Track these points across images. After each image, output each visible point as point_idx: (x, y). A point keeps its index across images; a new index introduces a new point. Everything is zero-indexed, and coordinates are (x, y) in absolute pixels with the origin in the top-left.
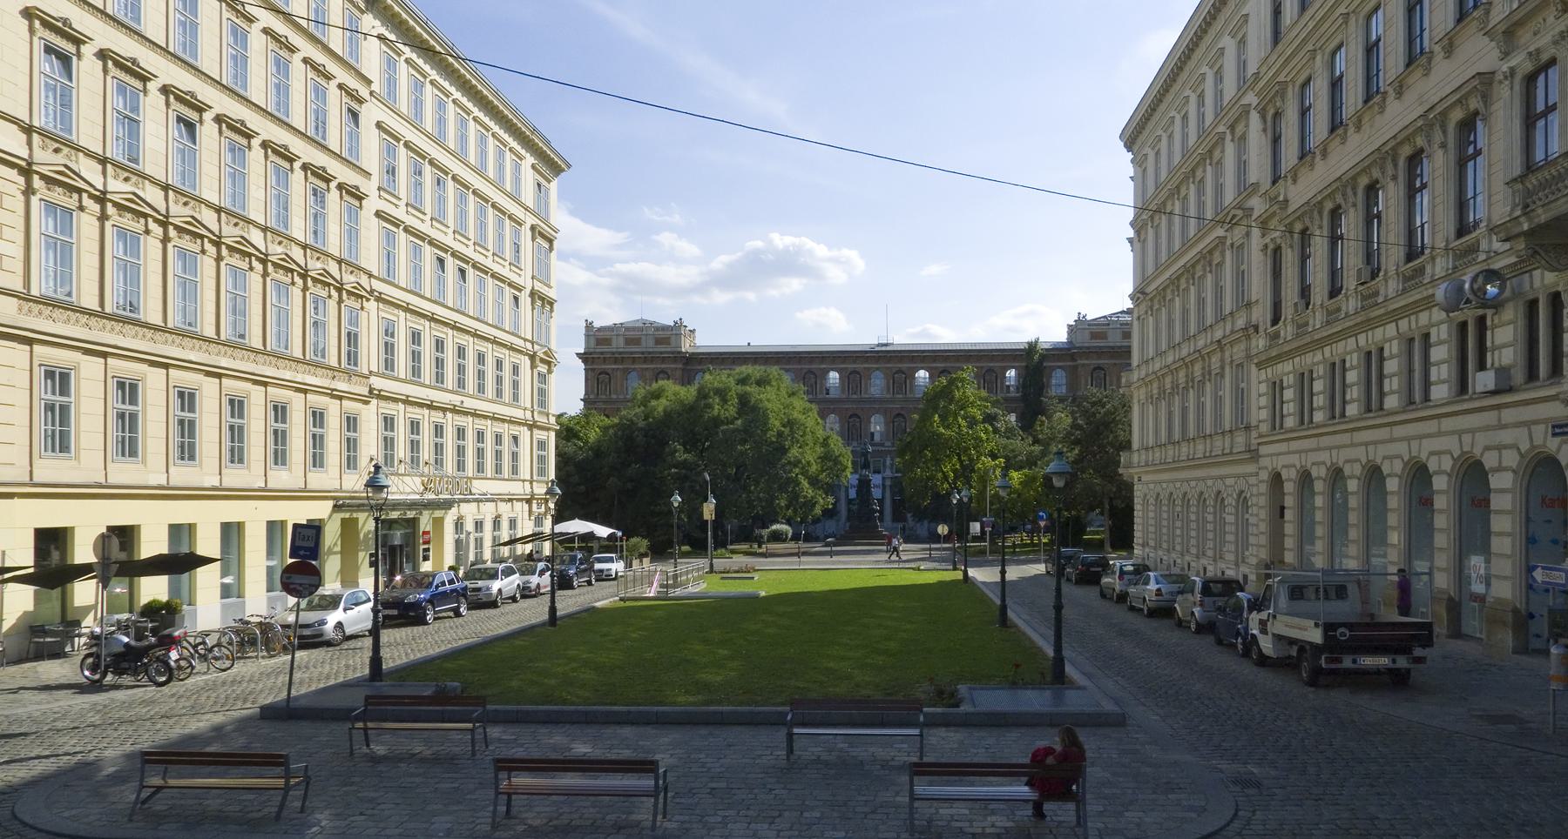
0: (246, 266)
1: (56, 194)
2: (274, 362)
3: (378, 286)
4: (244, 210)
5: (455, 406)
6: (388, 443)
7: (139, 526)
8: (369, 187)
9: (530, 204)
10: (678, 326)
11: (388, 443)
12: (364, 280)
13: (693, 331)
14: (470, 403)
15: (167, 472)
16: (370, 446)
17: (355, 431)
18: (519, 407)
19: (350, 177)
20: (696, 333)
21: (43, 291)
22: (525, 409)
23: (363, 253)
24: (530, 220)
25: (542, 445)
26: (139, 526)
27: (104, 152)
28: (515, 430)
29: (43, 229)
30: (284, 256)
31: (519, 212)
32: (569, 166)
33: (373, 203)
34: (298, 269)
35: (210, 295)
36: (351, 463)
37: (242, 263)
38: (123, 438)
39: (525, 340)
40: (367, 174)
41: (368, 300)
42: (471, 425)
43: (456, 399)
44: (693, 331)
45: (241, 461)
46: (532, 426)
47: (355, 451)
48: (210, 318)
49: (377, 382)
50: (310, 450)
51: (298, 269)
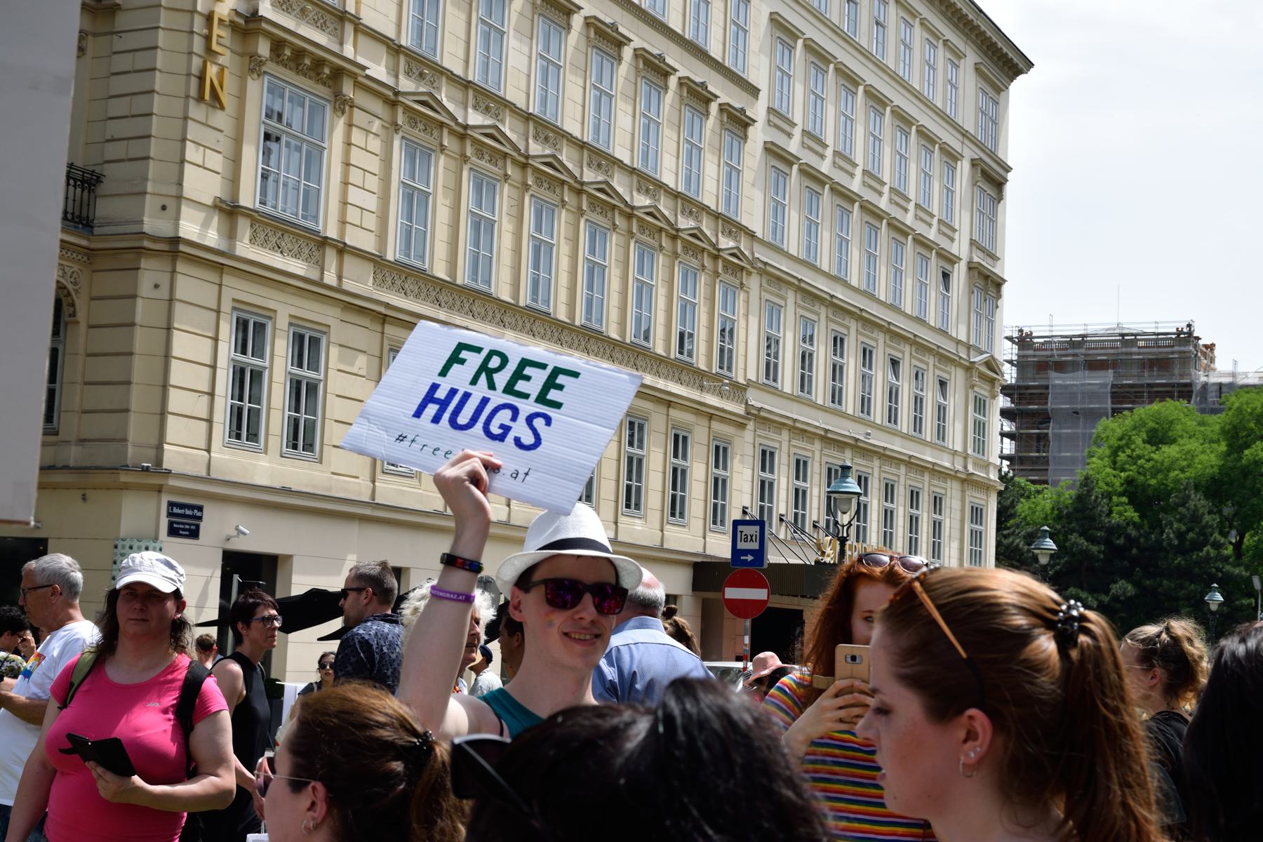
0: (656, 245)
1: (417, 131)
2: (273, 239)
3: (762, 254)
4: (656, 173)
5: (857, 440)
6: (765, 489)
7: (289, 558)
8: (758, 111)
9: (969, 126)
10: (1186, 337)
11: (765, 489)
12: (744, 245)
13: (1211, 347)
14: (878, 440)
15: (616, 523)
16: (742, 497)
17: (725, 468)
18: (943, 449)
19: (734, 97)
20: (1217, 352)
21: (397, 257)
22: (955, 453)
23: (745, 204)
24: (969, 153)
25: (977, 514)
26: (289, 558)
27: (528, 108)
28: (939, 486)
29: (402, 177)
30: (735, 251)
31: (954, 142)
32: (1031, 65)
33: (758, 135)
34: (571, 181)
35: (564, 263)
36: (717, 514)
37: (603, 219)
38: (240, 410)
39: (958, 342)
40: (754, 91)
41: (749, 273)
42: (926, 488)
43: (857, 431)
44: (1211, 347)
45: (309, 446)
46: (968, 481)
47: (639, 480)
48: (441, 251)
49: (756, 399)
50: (624, 482)
51: (571, 181)
